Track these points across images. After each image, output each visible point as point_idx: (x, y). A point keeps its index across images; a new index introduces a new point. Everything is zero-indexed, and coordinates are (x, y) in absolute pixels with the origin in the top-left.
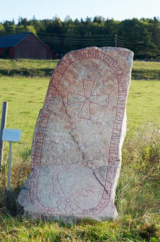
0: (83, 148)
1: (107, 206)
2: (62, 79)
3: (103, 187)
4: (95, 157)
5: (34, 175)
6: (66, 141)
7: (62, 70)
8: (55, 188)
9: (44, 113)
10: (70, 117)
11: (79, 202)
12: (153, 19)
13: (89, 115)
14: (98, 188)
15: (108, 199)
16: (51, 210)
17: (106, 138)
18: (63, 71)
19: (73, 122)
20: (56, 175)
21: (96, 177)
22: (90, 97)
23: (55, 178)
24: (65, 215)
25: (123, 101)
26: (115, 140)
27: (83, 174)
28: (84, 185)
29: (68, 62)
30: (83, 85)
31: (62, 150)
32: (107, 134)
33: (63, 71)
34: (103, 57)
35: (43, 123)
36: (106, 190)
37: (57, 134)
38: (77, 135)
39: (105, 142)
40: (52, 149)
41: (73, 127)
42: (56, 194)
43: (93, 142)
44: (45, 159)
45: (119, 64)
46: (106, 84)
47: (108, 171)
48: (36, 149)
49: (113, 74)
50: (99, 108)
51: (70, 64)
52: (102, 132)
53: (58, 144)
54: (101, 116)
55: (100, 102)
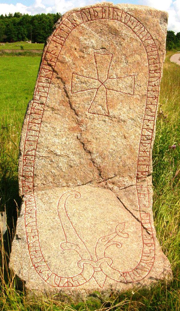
0: (98, 160)
1: (154, 258)
2: (61, 53)
3: (138, 223)
4: (117, 173)
5: (27, 209)
6: (72, 151)
7: (62, 38)
8: (67, 234)
9: (35, 108)
10: (77, 114)
11: (113, 259)
12: (56, 14)
13: (106, 108)
14: (132, 225)
15: (153, 245)
16: (72, 282)
17: (132, 143)
18: (63, 40)
19: (82, 122)
20: (64, 208)
21: (124, 206)
22: (107, 81)
23: (63, 214)
24: (98, 289)
25: (155, 85)
26: (145, 146)
27: (104, 202)
28: (111, 223)
29: (70, 25)
30: (96, 62)
31: (66, 166)
32: (133, 137)
33: (63, 40)
34: (125, 18)
35: (34, 124)
36: (144, 228)
37: (57, 141)
38: (89, 141)
39: (131, 150)
40: (51, 164)
41: (83, 129)
42: (72, 246)
43: (114, 151)
44: (41, 180)
45: (148, 30)
46: (130, 60)
47: (138, 193)
48: (25, 165)
49: (141, 45)
50: (121, 98)
51: (74, 28)
52: (126, 135)
53: (59, 156)
54: (125, 110)
55: (121, 88)
